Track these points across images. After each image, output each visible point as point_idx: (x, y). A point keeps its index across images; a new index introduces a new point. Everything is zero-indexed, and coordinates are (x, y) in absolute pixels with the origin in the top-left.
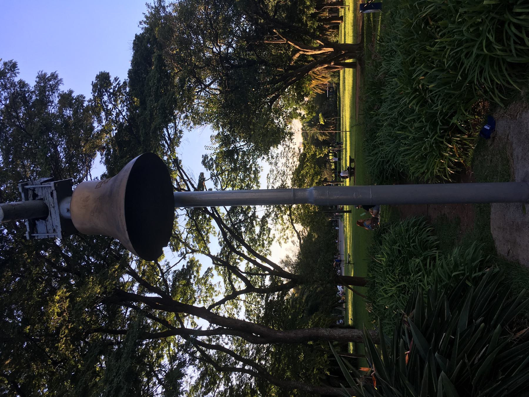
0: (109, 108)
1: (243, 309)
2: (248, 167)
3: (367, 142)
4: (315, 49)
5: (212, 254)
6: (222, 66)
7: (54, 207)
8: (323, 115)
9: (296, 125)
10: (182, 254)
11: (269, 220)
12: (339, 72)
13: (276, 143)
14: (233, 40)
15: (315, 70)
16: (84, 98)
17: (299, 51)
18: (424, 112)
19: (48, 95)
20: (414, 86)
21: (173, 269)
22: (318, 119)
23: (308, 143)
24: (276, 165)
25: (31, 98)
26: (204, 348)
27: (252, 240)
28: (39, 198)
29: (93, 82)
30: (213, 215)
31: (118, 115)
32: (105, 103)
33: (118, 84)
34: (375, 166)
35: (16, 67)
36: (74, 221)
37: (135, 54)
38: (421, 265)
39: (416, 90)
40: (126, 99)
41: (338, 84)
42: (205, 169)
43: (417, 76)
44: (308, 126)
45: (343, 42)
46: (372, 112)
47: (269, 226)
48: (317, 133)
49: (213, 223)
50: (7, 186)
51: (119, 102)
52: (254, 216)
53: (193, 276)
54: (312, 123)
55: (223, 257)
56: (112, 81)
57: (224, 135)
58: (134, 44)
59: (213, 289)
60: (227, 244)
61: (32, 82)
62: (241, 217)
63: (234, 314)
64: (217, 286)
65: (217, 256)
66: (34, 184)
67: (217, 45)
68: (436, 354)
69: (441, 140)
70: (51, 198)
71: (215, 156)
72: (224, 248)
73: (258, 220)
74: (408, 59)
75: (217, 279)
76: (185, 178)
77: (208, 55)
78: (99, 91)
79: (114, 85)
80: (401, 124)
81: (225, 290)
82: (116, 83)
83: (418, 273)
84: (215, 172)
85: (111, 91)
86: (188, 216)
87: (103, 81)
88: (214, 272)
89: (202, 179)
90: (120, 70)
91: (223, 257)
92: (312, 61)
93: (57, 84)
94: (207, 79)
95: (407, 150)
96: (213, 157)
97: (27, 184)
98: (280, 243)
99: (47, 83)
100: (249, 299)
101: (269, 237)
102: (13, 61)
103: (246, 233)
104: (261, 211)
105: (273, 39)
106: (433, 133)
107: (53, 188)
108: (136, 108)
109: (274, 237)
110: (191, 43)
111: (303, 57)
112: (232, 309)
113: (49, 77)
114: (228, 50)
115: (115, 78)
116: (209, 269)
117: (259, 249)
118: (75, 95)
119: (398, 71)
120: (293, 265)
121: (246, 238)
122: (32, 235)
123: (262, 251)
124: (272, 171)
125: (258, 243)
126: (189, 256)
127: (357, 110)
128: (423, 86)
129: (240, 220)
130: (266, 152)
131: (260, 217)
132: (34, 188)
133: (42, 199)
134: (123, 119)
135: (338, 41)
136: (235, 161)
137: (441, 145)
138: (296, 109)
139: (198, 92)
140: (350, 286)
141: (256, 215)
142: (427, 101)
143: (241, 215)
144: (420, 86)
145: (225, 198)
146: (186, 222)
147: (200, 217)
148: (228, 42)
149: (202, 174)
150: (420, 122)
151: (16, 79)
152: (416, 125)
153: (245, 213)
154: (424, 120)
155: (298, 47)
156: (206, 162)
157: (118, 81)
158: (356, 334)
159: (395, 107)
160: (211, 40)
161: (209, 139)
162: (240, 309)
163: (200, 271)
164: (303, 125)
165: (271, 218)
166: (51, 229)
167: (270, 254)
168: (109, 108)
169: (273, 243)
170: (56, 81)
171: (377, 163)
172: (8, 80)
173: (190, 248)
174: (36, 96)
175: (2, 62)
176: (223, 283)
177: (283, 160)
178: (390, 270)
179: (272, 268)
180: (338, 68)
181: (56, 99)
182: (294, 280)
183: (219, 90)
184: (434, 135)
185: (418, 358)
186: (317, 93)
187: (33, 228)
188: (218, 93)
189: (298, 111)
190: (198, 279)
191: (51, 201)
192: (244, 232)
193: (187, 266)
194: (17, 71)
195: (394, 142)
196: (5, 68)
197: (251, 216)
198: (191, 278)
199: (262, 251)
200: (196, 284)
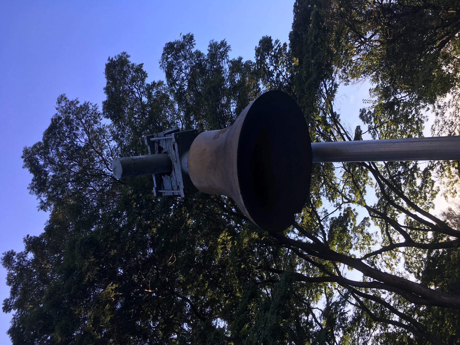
0: (270, 70)
1: (403, 261)
2: (410, 117)
5: (369, 205)
7: (176, 162)
10: (338, 204)
11: (433, 173)
13: (444, 92)
19: (219, 61)
21: (330, 217)
24: (443, 115)
25: (206, 65)
27: (413, 192)
28: (164, 151)
29: (256, 47)
30: (370, 168)
31: (278, 75)
33: (279, 46)
35: (193, 39)
37: (295, 17)
40: (286, 60)
42: (363, 123)
47: (433, 178)
49: (370, 174)
52: (415, 168)
53: (349, 224)
55: (380, 208)
56: (273, 44)
59: (370, 237)
60: (384, 196)
61: (205, 51)
62: (401, 169)
63: (392, 265)
65: (374, 206)
66: (159, 136)
70: (173, 151)
71: (373, 109)
72: (381, 199)
73: (420, 172)
75: (374, 228)
76: (342, 132)
78: (262, 55)
79: (275, 47)
81: (382, 240)
82: (277, 45)
84: (373, 124)
85: (273, 53)
86: (345, 168)
87: (266, 45)
88: (371, 221)
89: (358, 133)
90: (282, 34)
91: (380, 208)
93: (226, 51)
96: (371, 110)
97: (153, 137)
98: (446, 197)
99: (218, 50)
100: (409, 251)
101: (432, 190)
103: (406, 185)
104: (423, 165)
107: (174, 140)
109: (439, 190)
112: (391, 259)
115: (276, 41)
116: (366, 219)
117: (421, 201)
118: (244, 61)
120: (456, 217)
121: (406, 190)
123: (423, 204)
124: (437, 122)
125: (419, 196)
126: (345, 206)
129: (399, 172)
130: (432, 102)
131: (422, 169)
132: (159, 140)
133: (166, 153)
134: (283, 79)
136: (396, 113)
141: (418, 167)
143: (401, 167)
146: (343, 173)
147: (357, 168)
149: (358, 128)
151: (193, 50)
153: (405, 166)
156: (363, 116)
157: (278, 43)
162: (399, 260)
163: (356, 219)
165: (435, 170)
166: (174, 186)
167: (433, 208)
168: (270, 70)
169: (437, 196)
173: (346, 199)
175: (182, 36)
176: (381, 233)
179: (434, 223)
181: (226, 66)
190: (354, 226)
191: (174, 154)
192: (404, 184)
193: (344, 214)
194: (194, 43)
197: (412, 169)
198: (347, 225)
199: (423, 204)
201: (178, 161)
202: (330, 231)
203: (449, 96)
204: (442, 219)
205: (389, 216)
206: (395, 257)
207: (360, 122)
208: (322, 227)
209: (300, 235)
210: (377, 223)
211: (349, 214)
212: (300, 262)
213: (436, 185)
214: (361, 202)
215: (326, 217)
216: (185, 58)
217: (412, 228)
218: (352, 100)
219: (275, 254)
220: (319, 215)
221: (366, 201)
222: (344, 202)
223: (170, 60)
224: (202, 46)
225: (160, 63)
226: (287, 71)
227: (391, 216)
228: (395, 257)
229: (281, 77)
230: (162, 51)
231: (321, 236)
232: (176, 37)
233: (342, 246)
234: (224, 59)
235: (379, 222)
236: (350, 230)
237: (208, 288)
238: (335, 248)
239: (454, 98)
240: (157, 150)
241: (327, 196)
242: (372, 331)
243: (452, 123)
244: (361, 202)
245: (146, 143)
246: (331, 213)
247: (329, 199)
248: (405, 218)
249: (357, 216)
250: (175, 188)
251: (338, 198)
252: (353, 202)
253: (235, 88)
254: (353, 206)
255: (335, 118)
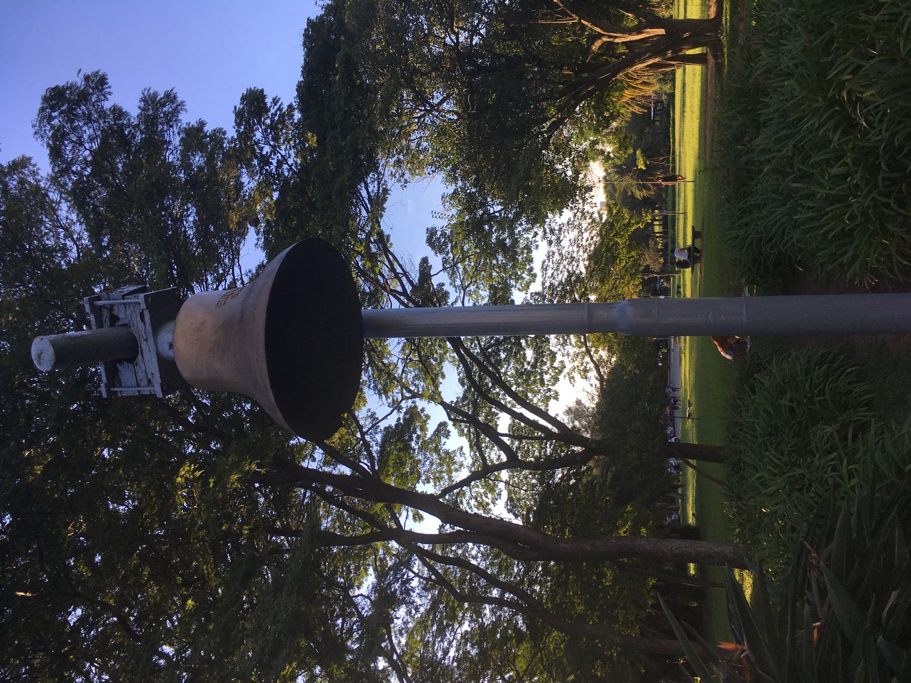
0: (264, 153)
1: (505, 495)
3: (729, 202)
4: (630, 31)
5: (447, 400)
6: (463, 70)
7: (146, 340)
8: (643, 152)
9: (596, 171)
12: (673, 73)
13: (559, 207)
14: (480, 21)
15: (630, 70)
16: (224, 133)
17: (600, 36)
18: (850, 145)
19: (162, 130)
20: (829, 95)
22: (633, 160)
23: (616, 204)
25: (134, 137)
26: (432, 562)
28: (121, 323)
29: (235, 108)
31: (280, 164)
32: (257, 143)
33: (280, 109)
34: (743, 246)
35: (106, 84)
36: (180, 368)
37: (307, 55)
38: (837, 440)
39: (833, 102)
41: (672, 96)
42: (433, 252)
43: (836, 75)
44: (617, 172)
45: (681, 17)
46: (739, 147)
48: (632, 185)
50: (105, 287)
51: (282, 140)
53: (414, 436)
54: (621, 168)
56: (269, 105)
57: (466, 194)
58: (306, 36)
61: (133, 109)
63: (488, 504)
64: (458, 454)
65: (457, 402)
67: (453, 32)
68: (880, 639)
69: (886, 200)
70: (140, 324)
74: (818, 41)
75: (456, 441)
76: (399, 270)
77: (437, 49)
78: (248, 123)
79: (273, 111)
80: (800, 170)
82: (276, 108)
83: (830, 453)
87: (254, 103)
90: (283, 83)
92: (624, 54)
93: (176, 112)
94: (435, 94)
95: (812, 219)
99: (160, 108)
102: (100, 73)
105: (552, 16)
106: (869, 187)
107: (143, 306)
108: (311, 150)
110: (406, 30)
111: (609, 47)
113: (161, 99)
114: (472, 40)
115: (274, 100)
116: (443, 425)
118: (209, 129)
119: (796, 66)
120: (588, 416)
122: (112, 389)
124: (550, 255)
127: (708, 143)
128: (849, 93)
133: (125, 325)
134: (289, 170)
135: (671, 16)
137: (886, 211)
138: (594, 143)
139: (419, 118)
140: (691, 461)
142: (858, 124)
144: (844, 94)
145: (463, 321)
148: (473, 26)
149: (425, 260)
150: (840, 166)
151: (107, 105)
152: (835, 170)
154: (849, 161)
155: (598, 30)
156: (433, 239)
158: (704, 550)
159: (788, 137)
160: (441, 24)
161: (440, 202)
164: (606, 170)
170: (174, 106)
171: (748, 242)
172: (94, 106)
173: (410, 391)
174: (142, 133)
175: (81, 75)
177: (573, 234)
178: (771, 444)
179: (555, 430)
180: (673, 65)
182: (592, 448)
183: (456, 113)
184: (870, 192)
185: (839, 637)
186: (633, 113)
187: (113, 377)
188: (455, 117)
189: (600, 147)
191: (142, 329)
193: (404, 419)
194: (108, 90)
195: (784, 204)
196: (87, 85)
198: (411, 439)
200: (420, 449)
201: (151, 340)
202: (381, 453)
203: (567, 214)
204: (564, 419)
205: (481, 419)
206: (492, 490)
207: (428, 252)
208: (367, 446)
209: (326, 463)
210: (463, 430)
211: (413, 418)
212: (329, 513)
213: (559, 357)
214: (435, 397)
215: (375, 426)
216: (89, 119)
217: (520, 438)
218: (414, 208)
219: (281, 503)
220: (362, 422)
221: (442, 395)
222: (404, 398)
223: (56, 122)
224: (126, 97)
225: (34, 126)
226: (296, 157)
227: (486, 417)
228: (492, 490)
229: (285, 166)
230: (38, 104)
231: (366, 461)
232: (68, 75)
233: (403, 477)
234: (172, 126)
235: (466, 430)
236: (416, 447)
237: (148, 581)
238: (392, 482)
239: (575, 216)
240: (108, 320)
241: (375, 387)
242: (456, 626)
243: (573, 258)
244: (435, 397)
245: (88, 310)
246: (383, 419)
247: (380, 395)
248: (510, 422)
249: (429, 421)
250: (145, 382)
251: (396, 391)
252: (421, 396)
253: (194, 182)
254: (421, 403)
255: (383, 240)
